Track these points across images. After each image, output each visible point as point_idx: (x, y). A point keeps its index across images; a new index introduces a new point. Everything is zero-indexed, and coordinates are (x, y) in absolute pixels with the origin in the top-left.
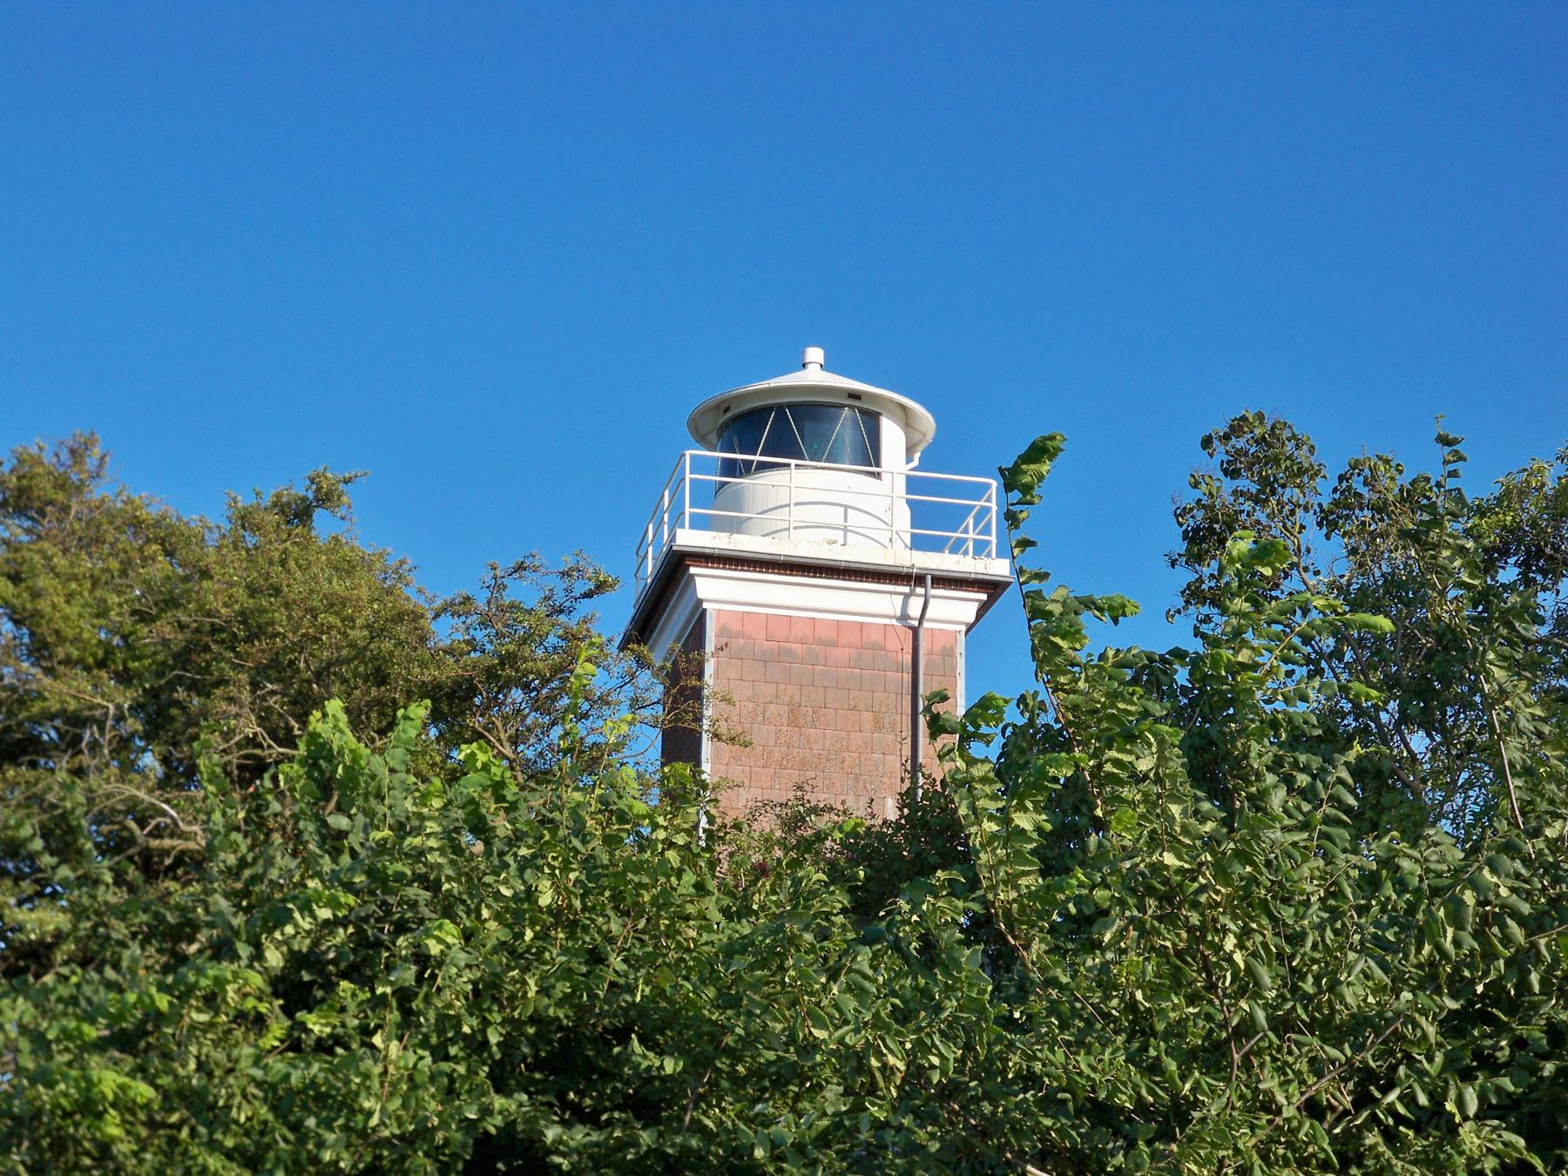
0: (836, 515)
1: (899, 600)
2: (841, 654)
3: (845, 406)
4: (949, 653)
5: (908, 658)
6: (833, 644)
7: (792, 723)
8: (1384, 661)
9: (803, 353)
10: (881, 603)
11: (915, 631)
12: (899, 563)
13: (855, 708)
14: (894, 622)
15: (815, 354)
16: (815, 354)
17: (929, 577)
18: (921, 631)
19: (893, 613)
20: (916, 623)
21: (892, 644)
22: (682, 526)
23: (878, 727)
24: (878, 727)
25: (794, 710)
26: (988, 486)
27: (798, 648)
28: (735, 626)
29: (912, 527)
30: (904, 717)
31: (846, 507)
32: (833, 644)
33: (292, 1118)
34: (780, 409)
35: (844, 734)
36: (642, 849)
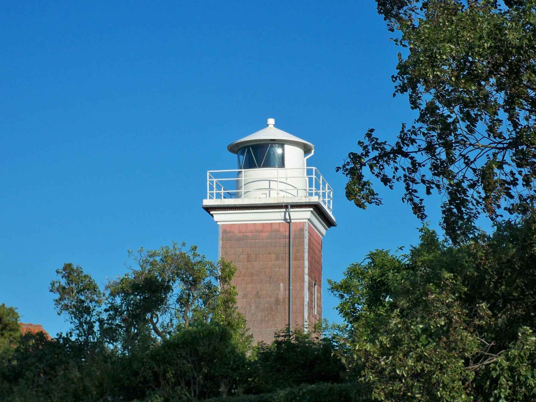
0: (266, 184)
1: (283, 214)
2: (264, 235)
3: (269, 144)
4: (302, 230)
5: (288, 234)
6: (262, 232)
7: (249, 260)
8: (414, 315)
9: (267, 121)
10: (277, 216)
11: (289, 223)
12: (279, 202)
13: (269, 253)
14: (283, 221)
15: (271, 121)
16: (271, 121)
17: (289, 206)
18: (291, 224)
19: (281, 219)
20: (289, 221)
21: (282, 229)
22: (206, 198)
23: (277, 259)
24: (277, 259)
25: (249, 256)
26: (312, 169)
27: (250, 235)
28: (228, 229)
29: (307, 166)
30: (286, 254)
31: (270, 181)
32: (262, 232)
33: (128, 382)
34: (248, 147)
35: (266, 263)
36: (459, 31)
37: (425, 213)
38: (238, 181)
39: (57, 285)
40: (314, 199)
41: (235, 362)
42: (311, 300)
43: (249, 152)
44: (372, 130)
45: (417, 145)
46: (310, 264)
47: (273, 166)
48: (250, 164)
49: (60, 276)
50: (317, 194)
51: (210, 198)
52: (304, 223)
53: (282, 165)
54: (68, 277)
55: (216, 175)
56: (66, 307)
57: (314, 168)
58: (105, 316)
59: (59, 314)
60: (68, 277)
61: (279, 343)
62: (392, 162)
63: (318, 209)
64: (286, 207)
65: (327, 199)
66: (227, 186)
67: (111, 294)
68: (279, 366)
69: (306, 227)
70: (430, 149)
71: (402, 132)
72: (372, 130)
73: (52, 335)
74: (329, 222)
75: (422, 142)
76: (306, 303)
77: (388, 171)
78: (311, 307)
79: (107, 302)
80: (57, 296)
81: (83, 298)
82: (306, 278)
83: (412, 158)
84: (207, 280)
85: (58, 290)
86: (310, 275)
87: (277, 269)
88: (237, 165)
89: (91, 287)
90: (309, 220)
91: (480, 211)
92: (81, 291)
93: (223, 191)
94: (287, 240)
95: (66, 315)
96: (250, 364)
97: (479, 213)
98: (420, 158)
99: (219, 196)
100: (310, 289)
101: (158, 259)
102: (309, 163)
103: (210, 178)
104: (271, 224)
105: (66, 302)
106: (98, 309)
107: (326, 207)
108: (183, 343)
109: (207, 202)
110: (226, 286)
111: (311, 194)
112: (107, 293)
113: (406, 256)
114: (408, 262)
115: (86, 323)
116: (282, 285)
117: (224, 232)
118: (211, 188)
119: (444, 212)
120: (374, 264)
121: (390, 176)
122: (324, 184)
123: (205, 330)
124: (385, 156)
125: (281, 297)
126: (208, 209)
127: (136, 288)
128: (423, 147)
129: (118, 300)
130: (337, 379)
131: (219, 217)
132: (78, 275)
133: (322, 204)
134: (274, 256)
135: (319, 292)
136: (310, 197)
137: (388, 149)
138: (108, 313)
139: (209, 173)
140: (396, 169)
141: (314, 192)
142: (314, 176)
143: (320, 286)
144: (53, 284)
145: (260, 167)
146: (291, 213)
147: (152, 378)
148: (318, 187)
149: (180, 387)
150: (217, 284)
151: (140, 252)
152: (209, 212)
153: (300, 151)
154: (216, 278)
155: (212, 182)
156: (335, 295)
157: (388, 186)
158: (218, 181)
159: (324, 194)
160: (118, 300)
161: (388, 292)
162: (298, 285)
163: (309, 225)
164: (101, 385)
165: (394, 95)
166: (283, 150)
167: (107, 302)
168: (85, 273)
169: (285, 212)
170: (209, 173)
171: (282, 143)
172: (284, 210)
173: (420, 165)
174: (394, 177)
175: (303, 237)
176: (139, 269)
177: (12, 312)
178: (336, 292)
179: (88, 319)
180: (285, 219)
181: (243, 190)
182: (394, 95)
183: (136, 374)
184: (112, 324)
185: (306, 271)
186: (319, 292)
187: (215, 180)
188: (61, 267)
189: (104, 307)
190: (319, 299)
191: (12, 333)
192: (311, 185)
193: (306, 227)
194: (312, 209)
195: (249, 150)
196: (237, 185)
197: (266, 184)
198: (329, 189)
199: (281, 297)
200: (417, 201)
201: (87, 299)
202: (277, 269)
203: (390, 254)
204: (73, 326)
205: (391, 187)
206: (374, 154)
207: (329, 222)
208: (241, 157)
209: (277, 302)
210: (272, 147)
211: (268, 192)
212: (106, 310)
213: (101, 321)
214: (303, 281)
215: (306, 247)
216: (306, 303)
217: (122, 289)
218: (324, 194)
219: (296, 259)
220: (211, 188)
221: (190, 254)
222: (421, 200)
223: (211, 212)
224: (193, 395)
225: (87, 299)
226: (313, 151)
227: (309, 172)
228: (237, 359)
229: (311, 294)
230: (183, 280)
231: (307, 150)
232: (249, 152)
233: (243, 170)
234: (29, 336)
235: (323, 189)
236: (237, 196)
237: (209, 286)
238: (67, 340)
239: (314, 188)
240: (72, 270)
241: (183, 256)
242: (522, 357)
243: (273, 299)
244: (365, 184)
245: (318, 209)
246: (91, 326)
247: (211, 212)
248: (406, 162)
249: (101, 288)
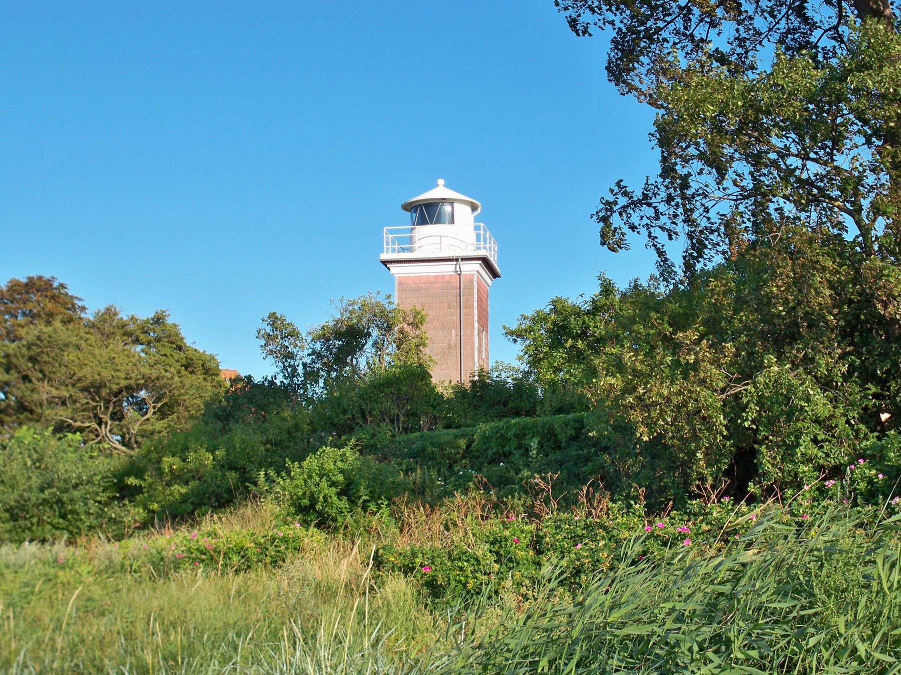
2: (437, 285)
4: (472, 281)
6: (434, 283)
10: (448, 269)
11: (460, 275)
15: (441, 182)
16: (441, 182)
21: (453, 280)
22: (383, 252)
23: (449, 308)
24: (449, 308)
27: (423, 285)
32: (434, 283)
34: (420, 206)
37: (667, 257)
38: (411, 237)
39: (262, 332)
40: (482, 253)
41: (435, 400)
42: (480, 345)
43: (421, 210)
44: (621, 181)
45: (660, 197)
46: (479, 311)
47: (444, 223)
48: (423, 222)
49: (265, 324)
50: (485, 248)
51: (387, 252)
52: (473, 275)
53: (452, 221)
54: (273, 324)
55: (391, 232)
56: (271, 352)
57: (482, 224)
58: (308, 360)
59: (264, 359)
60: (273, 324)
61: (473, 382)
62: (637, 210)
63: (486, 262)
64: (457, 260)
65: (492, 253)
66: (400, 241)
67: (313, 340)
68: (475, 403)
69: (475, 279)
70: (669, 199)
71: (646, 184)
72: (621, 181)
73: (257, 379)
74: (494, 274)
75: (663, 194)
76: (476, 348)
77: (635, 219)
78: (480, 352)
79: (308, 347)
80: (263, 342)
81: (287, 344)
82: (476, 324)
83: (655, 207)
84: (400, 325)
85: (263, 336)
86: (479, 322)
87: (449, 317)
88: (410, 222)
89: (294, 334)
90: (478, 272)
91: (713, 255)
92: (285, 337)
93: (397, 246)
94: (458, 290)
95: (271, 360)
96: (449, 401)
97: (713, 257)
98: (662, 208)
99: (393, 251)
100: (479, 335)
101: (356, 307)
102: (476, 219)
103: (387, 234)
104: (443, 276)
105: (271, 348)
106: (300, 354)
107: (492, 259)
108: (387, 383)
109: (385, 256)
110: (418, 332)
111: (478, 248)
112: (309, 339)
113: (586, 302)
114: (588, 308)
115: (290, 366)
116: (453, 331)
117: (400, 283)
118: (388, 244)
119: (684, 257)
120: (555, 310)
121: (636, 224)
122: (490, 239)
123: (408, 371)
124: (635, 204)
125: (452, 342)
126: (385, 263)
127: (338, 335)
128: (664, 199)
129: (318, 346)
130: (530, 413)
131: (395, 269)
132: (282, 323)
133: (489, 257)
134: (446, 305)
135: (486, 337)
136: (478, 251)
137: (635, 199)
138: (311, 357)
139: (386, 230)
140: (642, 217)
141: (482, 246)
142: (482, 232)
143: (487, 332)
144: (259, 332)
145: (431, 223)
146: (461, 266)
147: (359, 415)
148: (485, 241)
149: (385, 424)
150: (407, 328)
151: (341, 301)
152: (386, 266)
153: (469, 209)
154: (409, 324)
155: (388, 238)
156: (509, 339)
157: (636, 233)
158: (394, 237)
159: (490, 248)
160: (318, 346)
161: (570, 335)
162: (468, 331)
163: (478, 278)
164: (312, 422)
165: (653, 148)
166: (453, 208)
167: (308, 347)
168: (288, 321)
169: (456, 265)
170: (386, 230)
171: (451, 202)
172: (455, 263)
173: (661, 214)
174: (639, 225)
175: (472, 288)
176: (339, 316)
177: (212, 358)
178: (509, 337)
179: (292, 363)
180: (456, 271)
181: (416, 245)
182: (653, 148)
183: (345, 412)
184: (314, 367)
185: (476, 318)
186: (486, 337)
187: (390, 236)
188: (266, 316)
189: (306, 352)
190: (487, 344)
191: (213, 377)
192: (478, 239)
193: (475, 279)
194: (480, 262)
195: (422, 208)
196: (411, 240)
197: (437, 240)
198: (494, 243)
199: (452, 342)
200: (659, 246)
201: (290, 345)
202: (449, 317)
203: (570, 301)
204: (278, 370)
205: (638, 233)
206: (623, 201)
207: (494, 274)
208: (414, 215)
209: (450, 347)
210: (443, 205)
211: (439, 246)
212: (309, 355)
213: (304, 365)
214: (473, 328)
215: (476, 296)
216: (476, 348)
217: (324, 335)
218: (490, 248)
219: (466, 307)
220: (388, 244)
221: (385, 303)
222: (663, 246)
223: (388, 266)
224: (397, 430)
225: (290, 345)
226: (479, 209)
227: (477, 228)
228: (437, 397)
229: (480, 339)
230: (377, 326)
231: (474, 208)
232: (421, 210)
233: (417, 227)
234: (236, 380)
235: (490, 243)
236: (410, 250)
237: (401, 331)
238: (272, 383)
239: (482, 243)
240: (277, 318)
241: (378, 304)
242: (767, 384)
243: (446, 345)
244: (616, 229)
245: (486, 262)
246: (294, 369)
247: (388, 266)
248: (650, 212)
249: (303, 335)
